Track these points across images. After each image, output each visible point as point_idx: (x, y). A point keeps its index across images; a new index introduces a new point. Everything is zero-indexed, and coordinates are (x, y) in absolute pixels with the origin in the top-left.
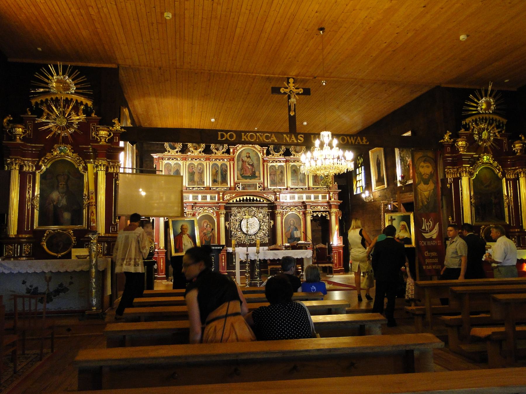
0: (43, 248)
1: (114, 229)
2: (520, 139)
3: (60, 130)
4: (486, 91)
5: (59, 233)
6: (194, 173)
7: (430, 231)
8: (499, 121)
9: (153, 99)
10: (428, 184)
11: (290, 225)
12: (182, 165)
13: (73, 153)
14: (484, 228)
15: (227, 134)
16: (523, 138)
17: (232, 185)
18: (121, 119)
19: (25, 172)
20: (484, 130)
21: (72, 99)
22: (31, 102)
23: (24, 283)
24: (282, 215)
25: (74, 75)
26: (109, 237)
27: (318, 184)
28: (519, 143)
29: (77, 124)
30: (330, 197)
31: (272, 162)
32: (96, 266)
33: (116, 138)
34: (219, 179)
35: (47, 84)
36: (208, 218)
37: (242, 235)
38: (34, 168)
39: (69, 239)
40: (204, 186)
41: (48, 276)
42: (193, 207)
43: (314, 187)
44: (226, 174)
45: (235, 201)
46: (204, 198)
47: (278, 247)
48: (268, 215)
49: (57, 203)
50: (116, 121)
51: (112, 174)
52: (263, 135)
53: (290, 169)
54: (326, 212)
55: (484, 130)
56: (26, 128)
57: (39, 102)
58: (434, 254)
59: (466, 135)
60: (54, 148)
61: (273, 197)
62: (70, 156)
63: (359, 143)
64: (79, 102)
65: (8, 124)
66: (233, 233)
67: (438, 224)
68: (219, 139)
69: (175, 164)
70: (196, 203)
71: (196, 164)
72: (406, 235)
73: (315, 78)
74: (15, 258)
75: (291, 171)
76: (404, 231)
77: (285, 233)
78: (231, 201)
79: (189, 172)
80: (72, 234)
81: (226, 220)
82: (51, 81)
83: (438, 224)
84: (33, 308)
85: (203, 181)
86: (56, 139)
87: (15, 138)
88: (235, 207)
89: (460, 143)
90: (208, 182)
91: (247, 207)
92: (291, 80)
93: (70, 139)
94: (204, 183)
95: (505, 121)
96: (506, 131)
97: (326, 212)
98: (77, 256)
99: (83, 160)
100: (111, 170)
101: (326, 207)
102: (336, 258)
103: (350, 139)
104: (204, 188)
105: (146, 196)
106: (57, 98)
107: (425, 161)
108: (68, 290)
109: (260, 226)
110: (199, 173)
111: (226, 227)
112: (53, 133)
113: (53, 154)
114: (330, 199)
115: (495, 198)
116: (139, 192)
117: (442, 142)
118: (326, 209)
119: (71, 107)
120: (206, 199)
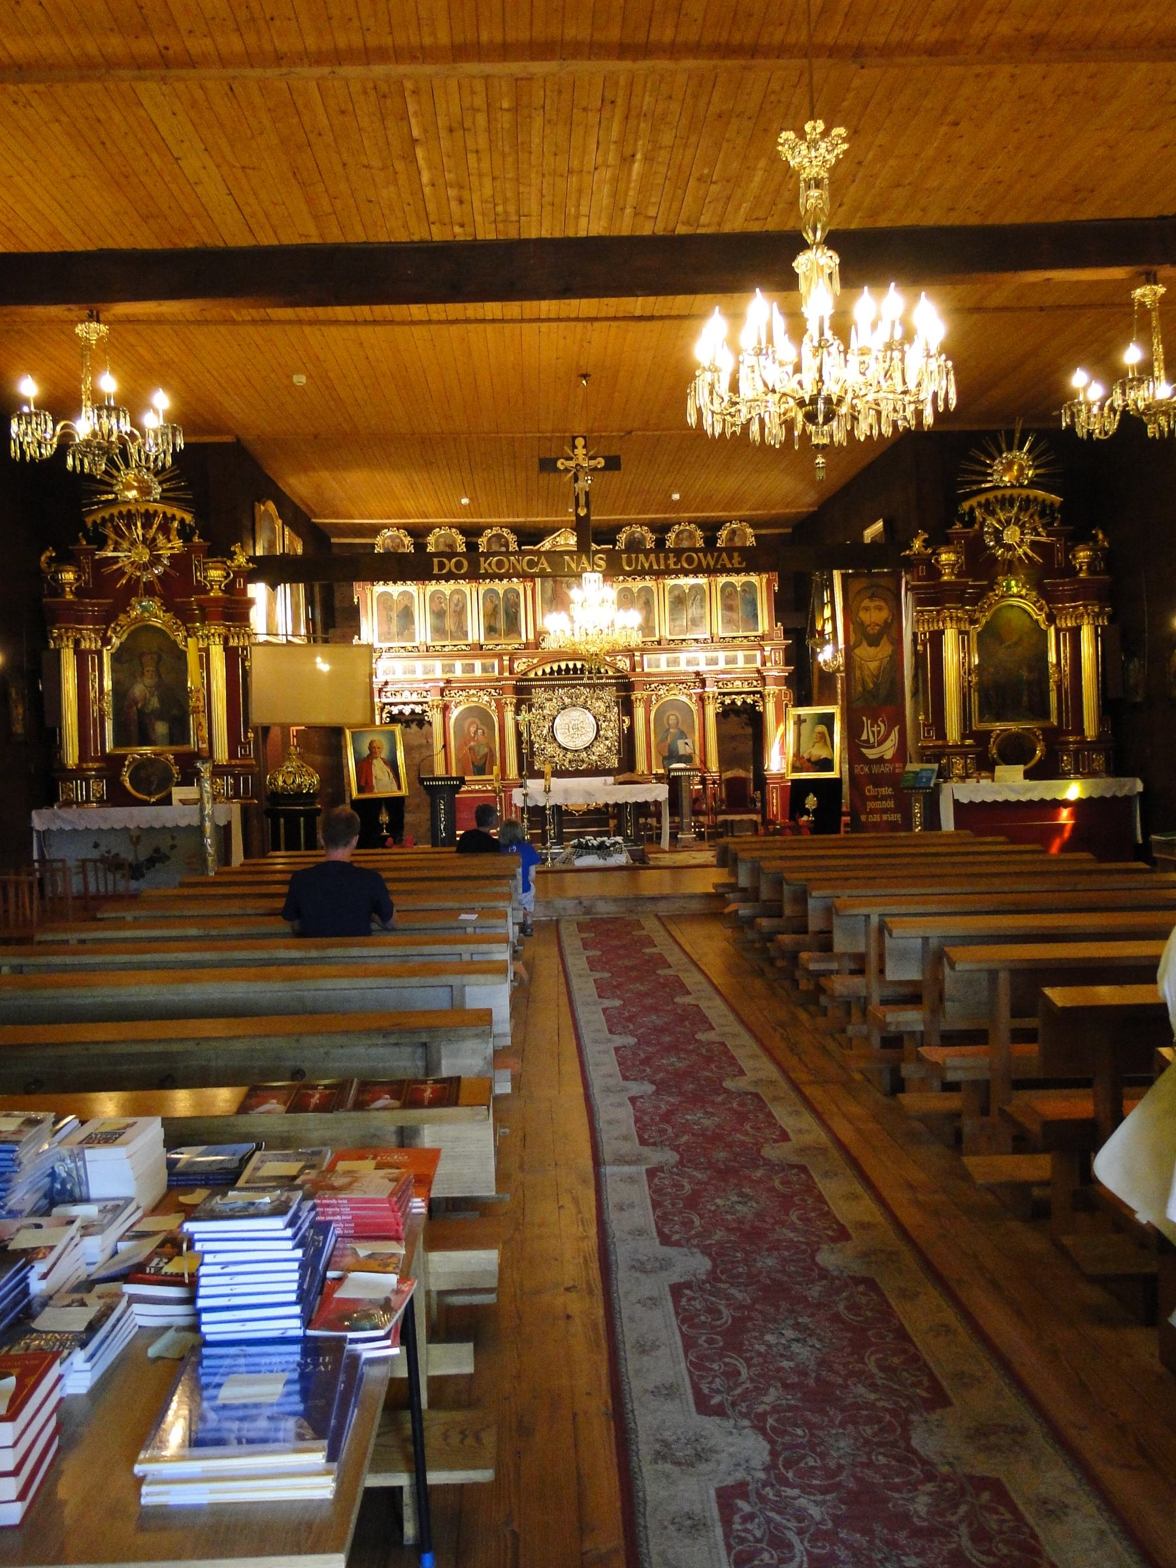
5: (149, 759)
6: (445, 612)
7: (880, 743)
9: (325, 475)
10: (877, 645)
12: (415, 595)
13: (165, 611)
15: (450, 561)
16: (1101, 536)
17: (531, 637)
18: (257, 536)
21: (156, 512)
23: (96, 846)
24: (648, 703)
26: (236, 766)
28: (1084, 550)
30: (763, 657)
32: (212, 818)
34: (501, 624)
35: (112, 485)
36: (480, 714)
37: (558, 750)
38: (100, 643)
39: (167, 770)
41: (134, 834)
42: (442, 690)
44: (517, 613)
45: (540, 673)
46: (470, 668)
47: (635, 778)
48: (617, 704)
49: (143, 706)
50: (236, 548)
51: (236, 648)
53: (667, 594)
54: (754, 693)
55: (1008, 522)
56: (79, 571)
57: (98, 521)
58: (886, 791)
59: (964, 536)
61: (628, 662)
62: (160, 618)
64: (169, 515)
65: (49, 567)
66: (536, 745)
67: (896, 728)
68: (436, 571)
70: (448, 681)
71: (448, 593)
72: (823, 753)
73: (630, 433)
74: (77, 803)
77: (657, 746)
78: (532, 675)
79: (433, 612)
83: (896, 728)
84: (110, 888)
86: (133, 588)
87: (64, 590)
88: (540, 686)
89: (944, 557)
90: (475, 631)
91: (567, 686)
92: (580, 442)
93: (158, 587)
94: (466, 633)
96: (1063, 522)
98: (180, 800)
99: (184, 624)
100: (233, 643)
101: (755, 683)
103: (705, 557)
105: (331, 672)
106: (129, 511)
107: (872, 597)
108: (168, 858)
109: (598, 731)
112: (127, 577)
114: (764, 663)
116: (315, 663)
117: (908, 556)
119: (155, 526)
120: (473, 671)
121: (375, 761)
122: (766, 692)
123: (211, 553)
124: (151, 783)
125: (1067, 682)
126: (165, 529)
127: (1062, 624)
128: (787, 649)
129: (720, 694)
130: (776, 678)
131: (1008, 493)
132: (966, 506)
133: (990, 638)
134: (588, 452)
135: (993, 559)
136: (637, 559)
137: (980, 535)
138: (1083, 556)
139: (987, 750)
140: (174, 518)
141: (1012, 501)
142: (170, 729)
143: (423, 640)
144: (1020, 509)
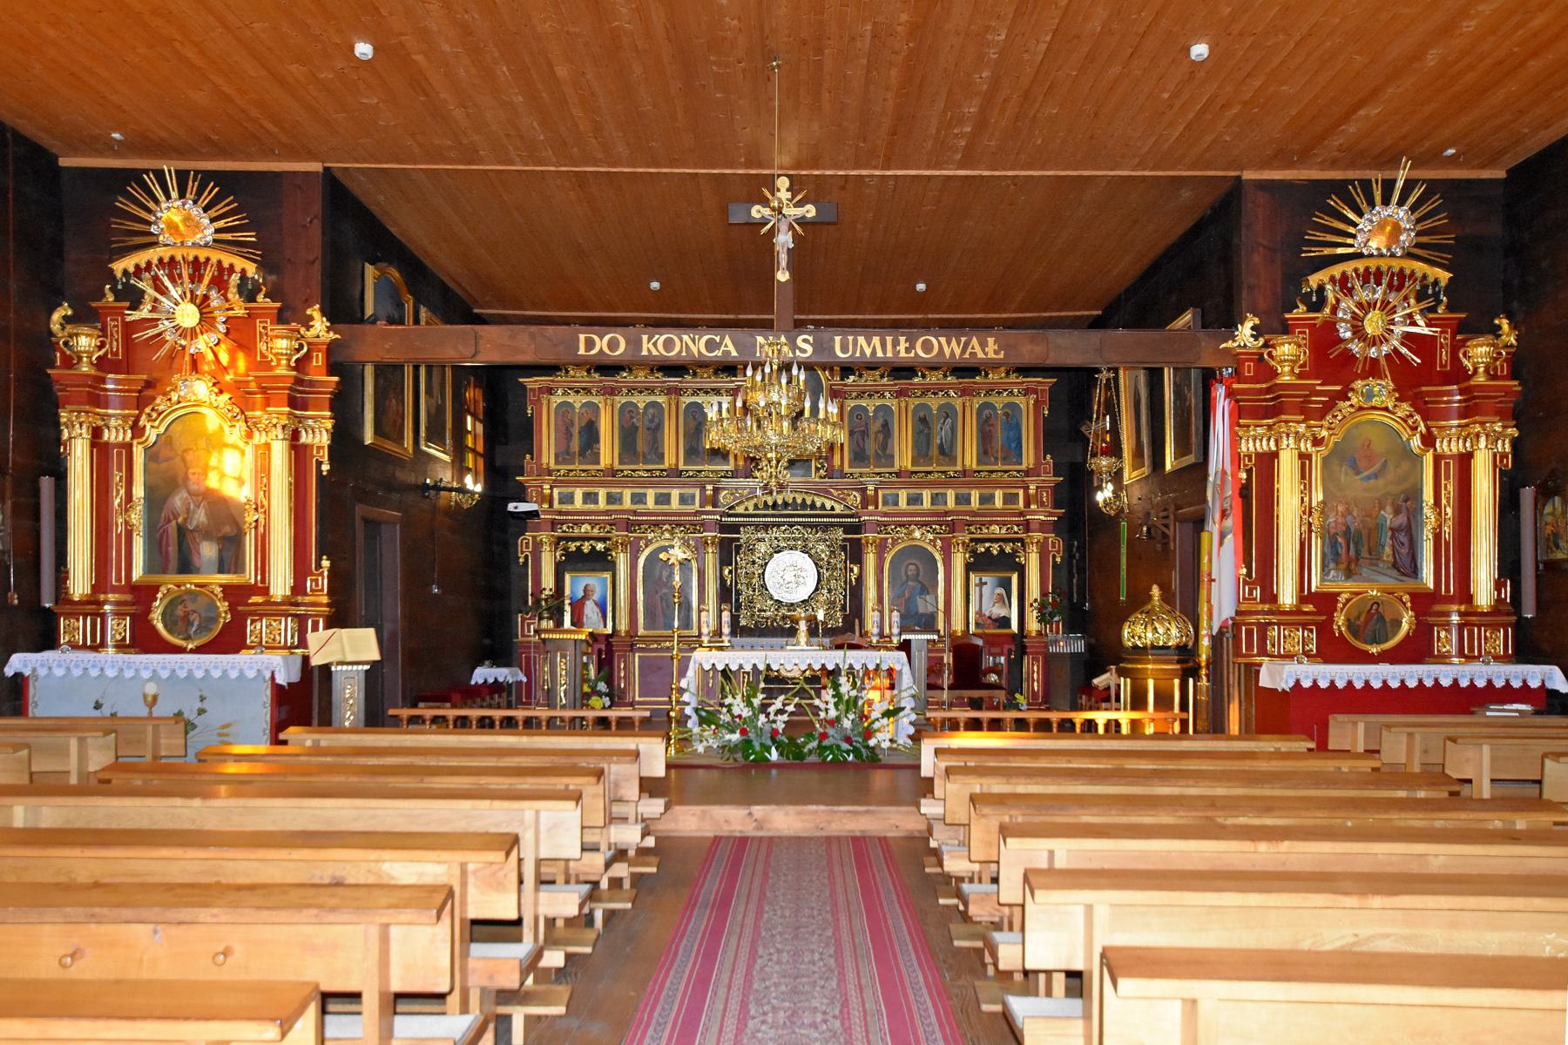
0: (154, 628)
1: (317, 585)
2: (1495, 331)
3: (185, 338)
4: (1388, 186)
6: (637, 428)
8: (1425, 277)
11: (904, 578)
14: (1348, 601)
16: (1506, 327)
19: (107, 444)
20: (1371, 305)
22: (112, 271)
24: (881, 548)
25: (206, 199)
27: (992, 459)
29: (224, 323)
31: (856, 398)
33: (317, 356)
40: (662, 467)
43: (980, 468)
52: (699, 339)
54: (1014, 540)
55: (1371, 305)
60: (171, 384)
63: (973, 354)
64: (226, 265)
65: (63, 328)
69: (584, 405)
71: (641, 405)
75: (913, 421)
76: (1001, 604)
78: (740, 510)
80: (220, 595)
81: (725, 560)
82: (155, 215)
85: (660, 451)
87: (80, 359)
95: (1444, 276)
96: (1450, 308)
97: (1014, 540)
101: (1016, 529)
102: (1035, 675)
103: (949, 343)
104: (662, 470)
110: (649, 429)
111: (722, 580)
113: (170, 399)
115: (1397, 512)
118: (1015, 533)
121: (587, 602)
122: (1028, 540)
123: (281, 318)
124: (190, 624)
125: (1448, 530)
126: (219, 283)
127: (1442, 446)
128: (1057, 488)
129: (972, 540)
130: (1042, 523)
131: (1372, 264)
132: (1314, 280)
133: (1345, 457)
134: (793, 197)
135: (1349, 357)
136: (855, 343)
137: (1331, 326)
138: (1479, 353)
139: (1331, 620)
140: (231, 269)
141: (1379, 275)
142: (220, 551)
143: (608, 462)
144: (1390, 286)
